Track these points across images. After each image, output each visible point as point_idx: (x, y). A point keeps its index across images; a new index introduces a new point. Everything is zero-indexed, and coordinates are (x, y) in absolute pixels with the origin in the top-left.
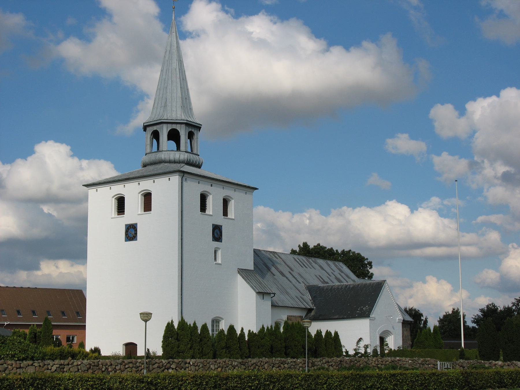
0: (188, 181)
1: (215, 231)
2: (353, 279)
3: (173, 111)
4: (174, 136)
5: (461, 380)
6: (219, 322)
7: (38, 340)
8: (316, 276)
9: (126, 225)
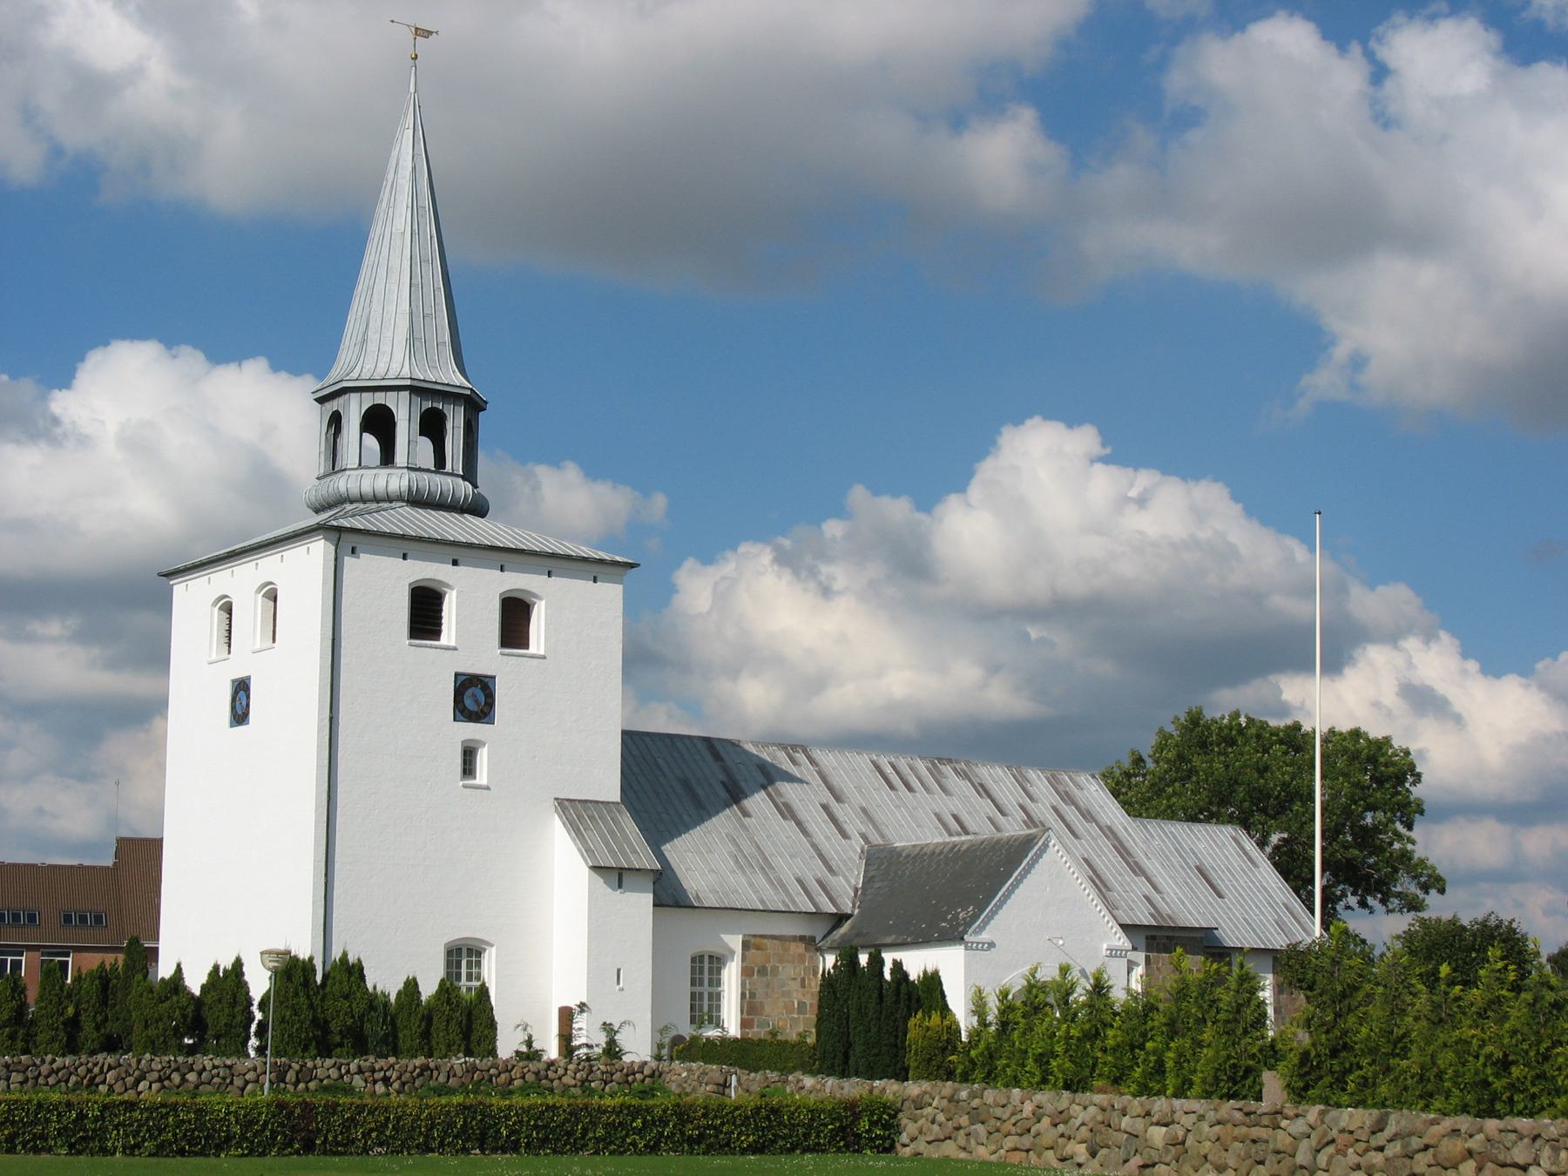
0: (361, 555)
1: (469, 692)
2: (1105, 819)
3: (384, 353)
4: (379, 423)
5: (471, 1131)
6: (479, 954)
7: (112, 999)
8: (938, 816)
9: (233, 681)
